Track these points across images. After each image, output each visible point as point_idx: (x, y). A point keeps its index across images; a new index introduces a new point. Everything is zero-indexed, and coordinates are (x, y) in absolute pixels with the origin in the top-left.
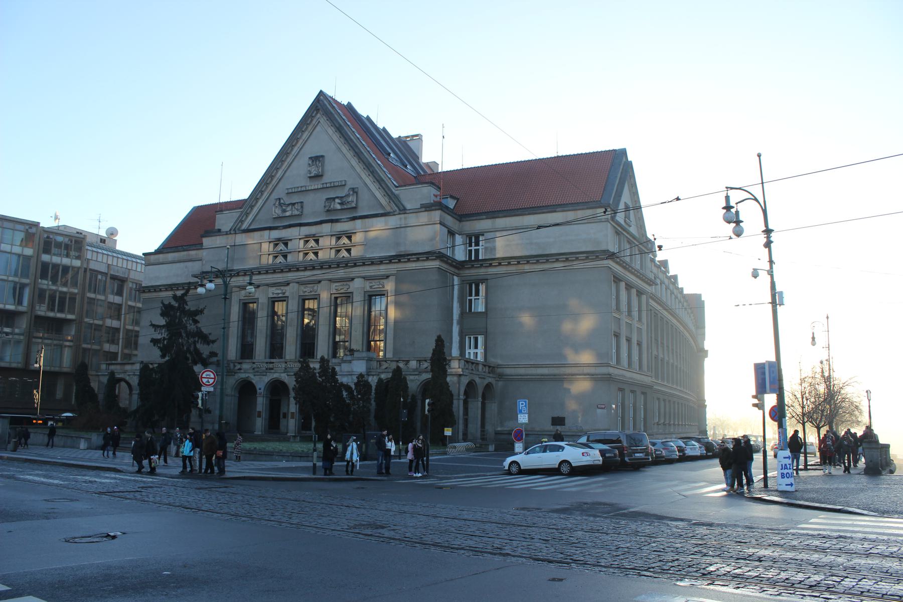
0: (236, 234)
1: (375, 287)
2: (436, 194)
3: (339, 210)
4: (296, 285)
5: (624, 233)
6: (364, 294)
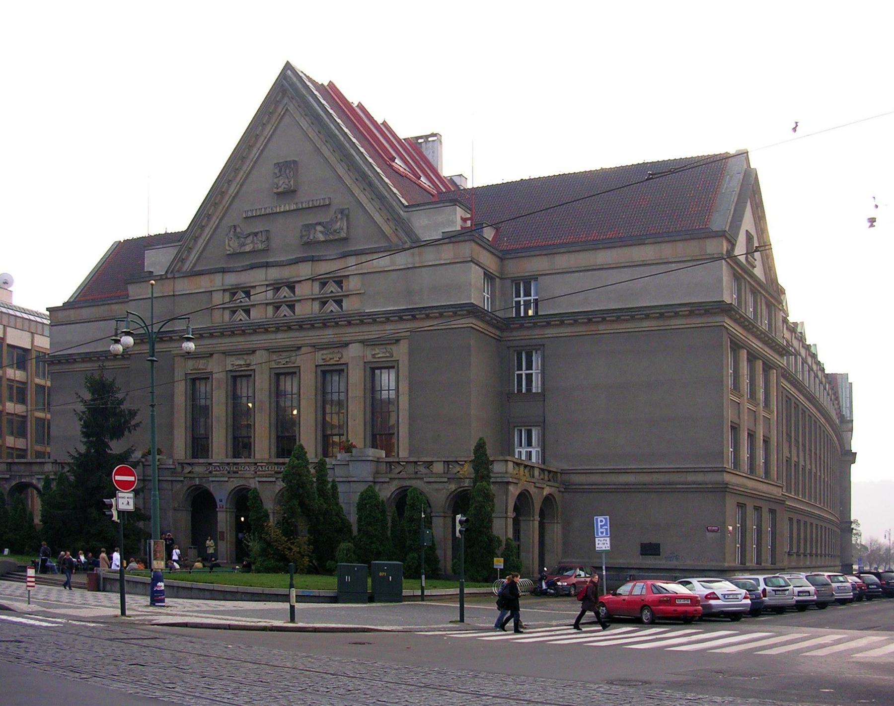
0: (174, 278)
1: (379, 356)
2: (464, 217)
3: (323, 241)
4: (264, 354)
5: (746, 276)
6: (365, 366)
